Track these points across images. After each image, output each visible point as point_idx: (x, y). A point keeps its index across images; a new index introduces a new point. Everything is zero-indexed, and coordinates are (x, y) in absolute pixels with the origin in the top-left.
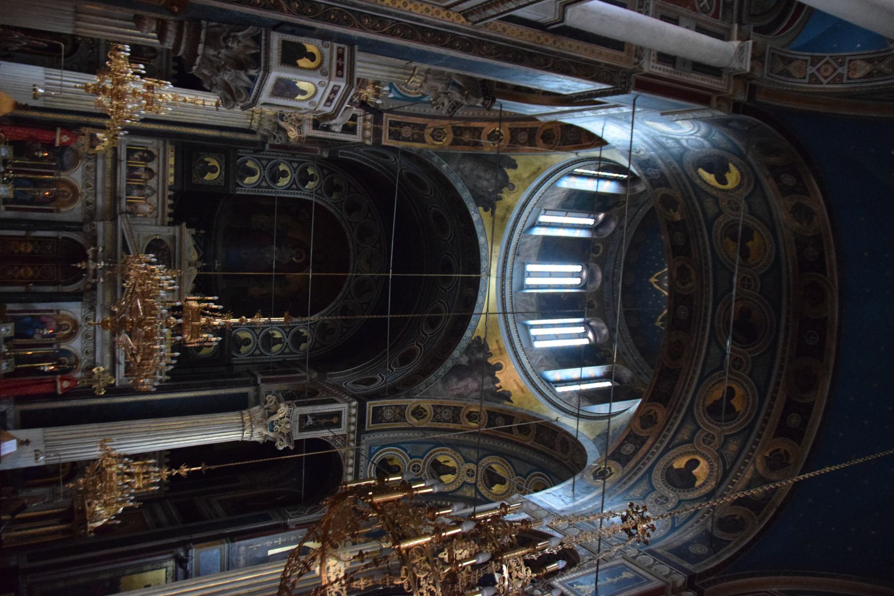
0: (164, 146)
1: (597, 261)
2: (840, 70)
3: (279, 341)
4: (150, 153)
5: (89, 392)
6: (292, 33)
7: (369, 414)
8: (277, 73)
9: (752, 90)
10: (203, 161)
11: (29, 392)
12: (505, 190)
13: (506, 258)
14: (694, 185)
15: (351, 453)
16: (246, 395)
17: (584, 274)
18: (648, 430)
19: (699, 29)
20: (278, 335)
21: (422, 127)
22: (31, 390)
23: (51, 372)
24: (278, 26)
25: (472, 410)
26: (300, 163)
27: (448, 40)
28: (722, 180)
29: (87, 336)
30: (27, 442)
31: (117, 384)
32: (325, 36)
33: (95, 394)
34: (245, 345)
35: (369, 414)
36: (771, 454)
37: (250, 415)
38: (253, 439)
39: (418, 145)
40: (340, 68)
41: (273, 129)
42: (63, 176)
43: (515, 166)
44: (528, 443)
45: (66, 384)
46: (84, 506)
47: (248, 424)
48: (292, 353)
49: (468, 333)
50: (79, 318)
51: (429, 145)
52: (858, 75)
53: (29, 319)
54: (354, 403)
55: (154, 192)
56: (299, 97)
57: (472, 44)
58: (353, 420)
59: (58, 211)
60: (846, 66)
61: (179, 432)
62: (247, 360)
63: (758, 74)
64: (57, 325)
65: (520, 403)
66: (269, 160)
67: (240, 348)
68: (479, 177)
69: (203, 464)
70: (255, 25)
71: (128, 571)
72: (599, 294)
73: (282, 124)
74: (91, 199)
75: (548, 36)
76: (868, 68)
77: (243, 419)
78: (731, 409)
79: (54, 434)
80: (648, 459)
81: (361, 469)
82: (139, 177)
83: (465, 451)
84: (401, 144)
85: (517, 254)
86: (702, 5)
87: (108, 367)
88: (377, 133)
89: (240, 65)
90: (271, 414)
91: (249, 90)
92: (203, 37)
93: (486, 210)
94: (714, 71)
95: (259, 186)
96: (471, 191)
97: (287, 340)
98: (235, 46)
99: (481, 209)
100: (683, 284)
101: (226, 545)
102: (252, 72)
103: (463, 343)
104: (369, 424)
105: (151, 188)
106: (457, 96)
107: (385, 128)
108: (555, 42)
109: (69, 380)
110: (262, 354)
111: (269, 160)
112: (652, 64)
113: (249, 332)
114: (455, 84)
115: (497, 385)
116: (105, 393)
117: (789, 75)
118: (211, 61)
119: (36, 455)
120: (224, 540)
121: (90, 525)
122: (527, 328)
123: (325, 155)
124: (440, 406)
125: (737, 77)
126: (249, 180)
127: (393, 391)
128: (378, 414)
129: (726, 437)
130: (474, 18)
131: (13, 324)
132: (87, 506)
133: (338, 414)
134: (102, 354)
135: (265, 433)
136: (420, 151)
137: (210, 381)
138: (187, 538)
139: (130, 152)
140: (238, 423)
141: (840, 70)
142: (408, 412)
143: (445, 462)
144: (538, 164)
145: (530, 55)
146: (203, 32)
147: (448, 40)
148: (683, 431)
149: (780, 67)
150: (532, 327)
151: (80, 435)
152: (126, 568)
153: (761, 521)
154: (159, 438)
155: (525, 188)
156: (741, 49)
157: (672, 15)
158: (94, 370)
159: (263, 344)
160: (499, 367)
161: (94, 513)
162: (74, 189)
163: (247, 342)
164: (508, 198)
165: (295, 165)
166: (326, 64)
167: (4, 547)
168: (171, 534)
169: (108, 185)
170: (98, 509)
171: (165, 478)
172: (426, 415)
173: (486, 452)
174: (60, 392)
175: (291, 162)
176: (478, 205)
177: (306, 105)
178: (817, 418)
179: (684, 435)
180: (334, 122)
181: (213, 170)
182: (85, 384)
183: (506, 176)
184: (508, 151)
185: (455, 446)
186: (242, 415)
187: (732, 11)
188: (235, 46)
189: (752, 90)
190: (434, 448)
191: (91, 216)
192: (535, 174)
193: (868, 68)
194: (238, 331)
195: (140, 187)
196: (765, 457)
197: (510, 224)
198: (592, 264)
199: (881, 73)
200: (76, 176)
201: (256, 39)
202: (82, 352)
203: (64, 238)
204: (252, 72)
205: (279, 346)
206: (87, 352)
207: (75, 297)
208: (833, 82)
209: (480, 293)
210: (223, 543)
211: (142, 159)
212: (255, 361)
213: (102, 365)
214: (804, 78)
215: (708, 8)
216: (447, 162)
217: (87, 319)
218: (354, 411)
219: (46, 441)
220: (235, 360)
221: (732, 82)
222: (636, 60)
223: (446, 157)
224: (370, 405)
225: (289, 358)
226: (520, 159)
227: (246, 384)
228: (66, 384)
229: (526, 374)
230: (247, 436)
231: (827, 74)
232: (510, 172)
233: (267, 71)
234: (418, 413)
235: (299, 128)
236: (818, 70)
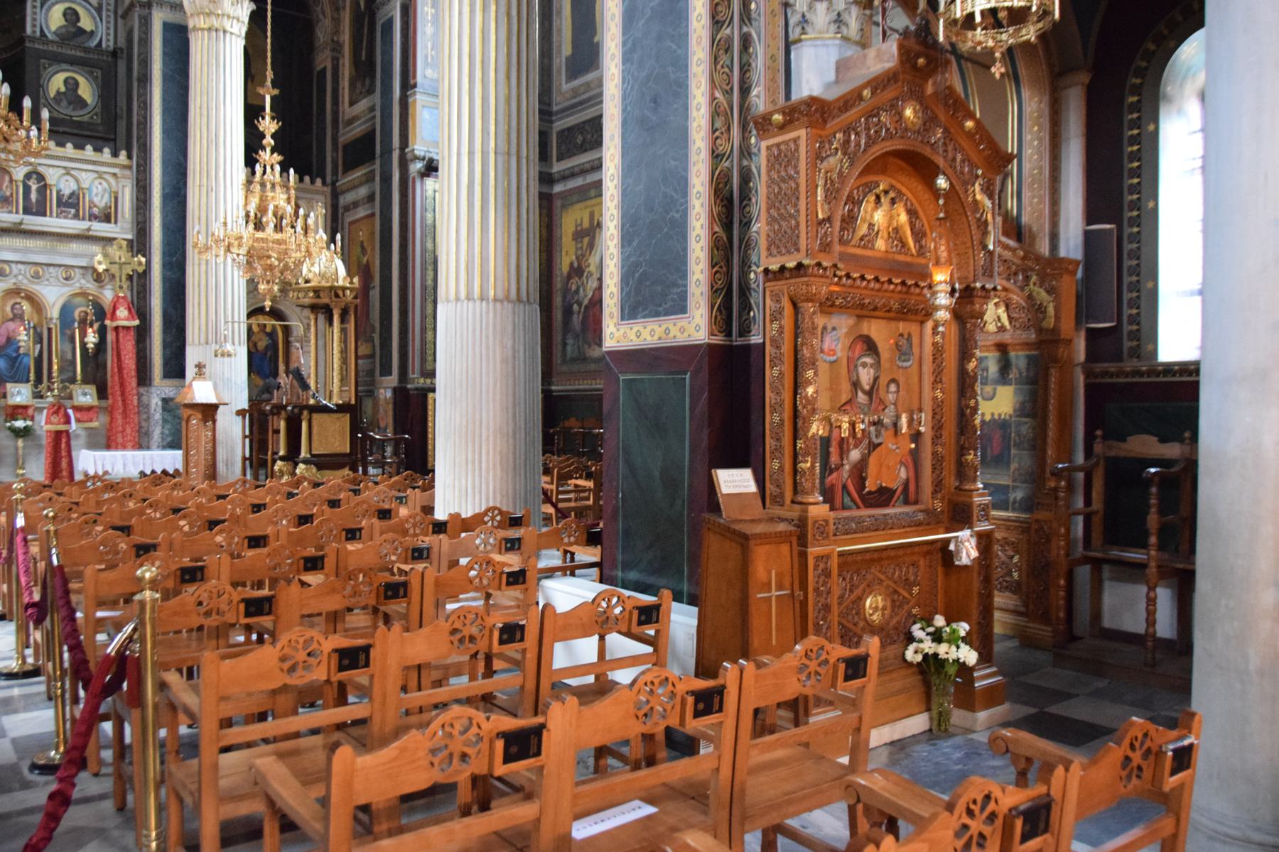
5: (140, 281)
11: (134, 367)
16: (167, 27)
22: (130, 362)
23: (102, 332)
29: (37, 276)
30: (200, 366)
31: (130, 237)
33: (145, 272)
34: (78, 19)
37: (199, 14)
38: (246, 20)
45: (122, 312)
46: (309, 289)
47: (215, 22)
61: (214, 142)
62: (108, 22)
64: (12, 320)
67: (82, 31)
69: (261, 91)
71: (429, 245)
77: (203, 29)
79: (196, 331)
87: (96, 248)
101: (418, 97)
109: (115, 309)
113: (50, 8)
116: (144, 256)
119: (223, 355)
120: (410, 100)
121: (341, 283)
131: (9, 386)
132: (308, 285)
134: (74, 254)
137: (135, 84)
138: (396, 155)
140: (209, 39)
151: (203, 294)
152: (424, 250)
154: (221, 174)
158: (101, 268)
161: (322, 276)
167: (353, 402)
168: (386, 179)
170: (316, 269)
171: (277, 158)
174: (137, 322)
182: (125, 285)
186: (195, 29)
194: (48, 27)
202: (67, 285)
206: (66, 279)
210: (415, 101)
212: (112, 8)
213: (93, 256)
220: (108, 44)
227: (146, 23)
228: (122, 312)
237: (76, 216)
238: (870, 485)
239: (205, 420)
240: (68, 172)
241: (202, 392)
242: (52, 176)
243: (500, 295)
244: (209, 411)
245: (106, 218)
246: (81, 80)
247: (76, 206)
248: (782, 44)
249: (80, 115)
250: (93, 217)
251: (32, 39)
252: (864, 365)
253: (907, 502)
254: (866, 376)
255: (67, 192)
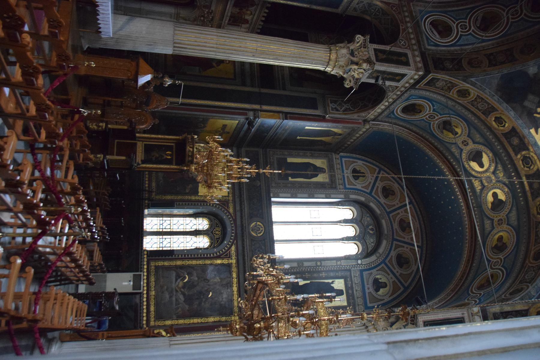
7: (427, 79)
25: (503, 117)
35: (427, 79)
71: (215, 118)
83: (473, 131)
124: (482, 99)
143: (454, 126)
172: (467, 97)
173: (485, 218)
185: (469, 124)
190: (455, 115)
219: (174, 43)
230: (328, 69)
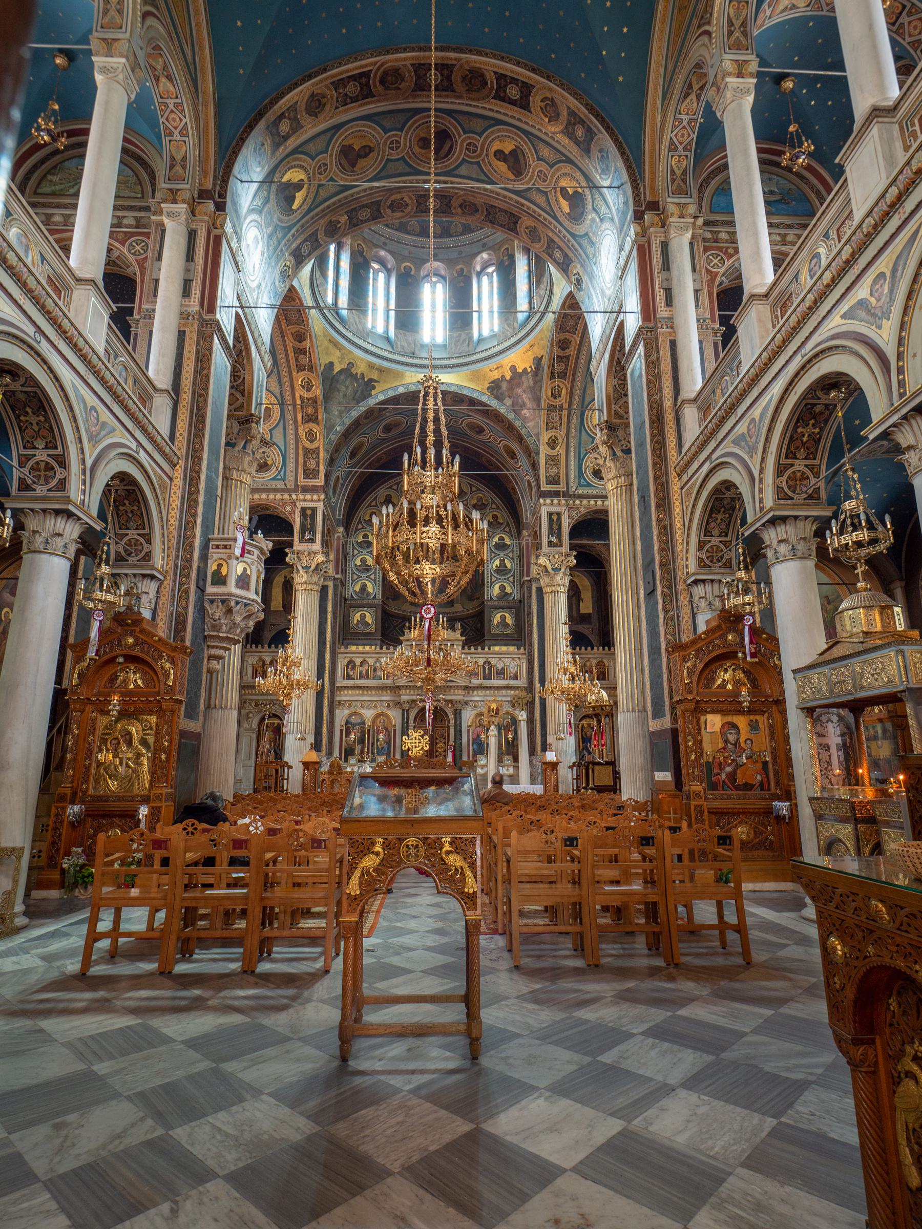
0: (342, 653)
1: (418, 269)
2: (171, 106)
3: (502, 561)
4: (349, 663)
6: (205, 580)
8: (232, 587)
9: (204, 194)
10: (357, 624)
12: (354, 371)
13: (416, 366)
14: (310, 210)
15: (585, 502)
17: (434, 279)
18: (542, 235)
19: (159, 258)
20: (497, 562)
21: (306, 450)
24: (201, 589)
26: (354, 548)
27: (194, 474)
28: (299, 186)
32: (204, 557)
36: (546, 116)
38: (567, 584)
39: (322, 450)
40: (225, 547)
41: (318, 574)
42: (368, 723)
43: (331, 364)
44: (578, 340)
48: (513, 551)
49: (484, 399)
50: (475, 712)
51: (320, 443)
52: (171, 88)
53: (475, 746)
54: (541, 501)
55: (378, 660)
56: (248, 572)
57: (195, 455)
58: (556, 501)
59: (395, 726)
60: (168, 101)
63: (187, 195)
65: (543, 348)
66: (353, 573)
67: (507, 594)
68: (345, 395)
70: (203, 602)
72: (450, 263)
73: (313, 567)
74: (385, 704)
75: (181, 399)
76: (163, 80)
78: (514, 153)
80: (565, 237)
81: (599, 493)
82: (367, 671)
84: (322, 468)
85: (413, 355)
86: (142, 252)
88: (313, 489)
89: (229, 611)
90: (547, 571)
91: (246, 605)
92: (215, 634)
93: (374, 388)
94: (192, 235)
95: (375, 580)
96: (358, 402)
97: (502, 554)
98: (218, 614)
99: (373, 392)
100: (407, 205)
102: (233, 604)
103: (494, 404)
104: (561, 487)
105: (375, 663)
106: (255, 443)
107: (311, 483)
108: (185, 393)
110: (513, 575)
111: (353, 573)
112: (192, 303)
114: (244, 447)
115: (529, 370)
117: (184, 159)
118: (230, 628)
122: (481, 340)
123: (341, 529)
125: (193, 213)
126: (370, 589)
127: (535, 466)
128: (554, 480)
129: (539, 159)
130: (175, 459)
133: (550, 514)
135: (561, 575)
136: (326, 451)
139: (349, 677)
141: (171, 106)
142: (552, 453)
144: (326, 343)
145: (198, 409)
146: (212, 633)
147: (194, 474)
148: (538, 201)
149: (178, 168)
150: (480, 335)
153: (602, 133)
155: (350, 352)
156: (169, 215)
157: (152, 286)
159: (505, 575)
160: (513, 368)
162: (378, 716)
163: (502, 588)
164: (360, 369)
165: (356, 552)
166: (225, 557)
169: (374, 692)
175: (353, 556)
176: (370, 395)
177: (254, 568)
178: (508, 68)
179: (541, 200)
180: (265, 549)
181: (363, 617)
183: (341, 371)
184: (317, 372)
187: (142, 217)
188: (218, 614)
189: (204, 194)
191: (398, 704)
192: (336, 344)
193: (163, 80)
195: (375, 670)
196: (549, 121)
197: (386, 364)
198: (423, 273)
199: (165, 68)
200: (368, 715)
201: (212, 601)
203: (415, 722)
204: (233, 604)
205: (506, 561)
207: (458, 714)
208: (182, 111)
209: (449, 389)
211: (353, 668)
214: (185, 142)
215: (143, 244)
216: (333, 426)
217: (475, 707)
218: (548, 501)
221: (199, 217)
222: (191, 318)
223: (329, 428)
224: (544, 487)
225: (517, 553)
226: (325, 360)
227: (529, 588)
229: (519, 342)
231: (178, 120)
232: (337, 368)
233: (231, 595)
234: (553, 443)
235: (315, 554)
236: (176, 128)
237: (504, 679)
238: (739, 781)
239: (553, 770)
240: (500, 659)
241: (550, 756)
242: (494, 662)
243: (641, 709)
244: (554, 766)
245: (516, 677)
246: (507, 615)
247: (504, 674)
248: (690, 615)
249: (508, 631)
250: (511, 678)
251: (487, 601)
252: (731, 733)
253: (762, 789)
254: (732, 738)
255: (500, 668)
